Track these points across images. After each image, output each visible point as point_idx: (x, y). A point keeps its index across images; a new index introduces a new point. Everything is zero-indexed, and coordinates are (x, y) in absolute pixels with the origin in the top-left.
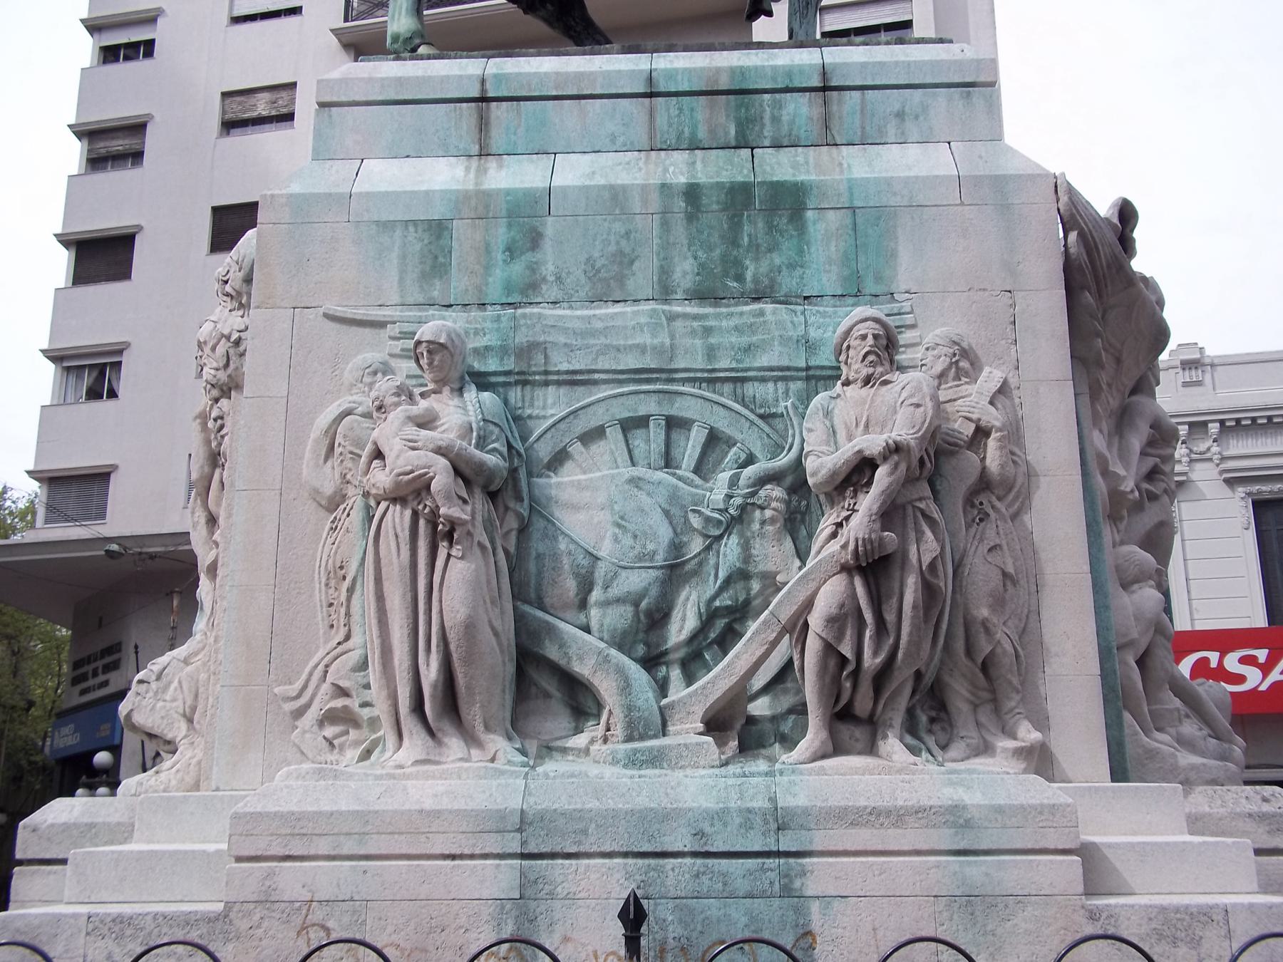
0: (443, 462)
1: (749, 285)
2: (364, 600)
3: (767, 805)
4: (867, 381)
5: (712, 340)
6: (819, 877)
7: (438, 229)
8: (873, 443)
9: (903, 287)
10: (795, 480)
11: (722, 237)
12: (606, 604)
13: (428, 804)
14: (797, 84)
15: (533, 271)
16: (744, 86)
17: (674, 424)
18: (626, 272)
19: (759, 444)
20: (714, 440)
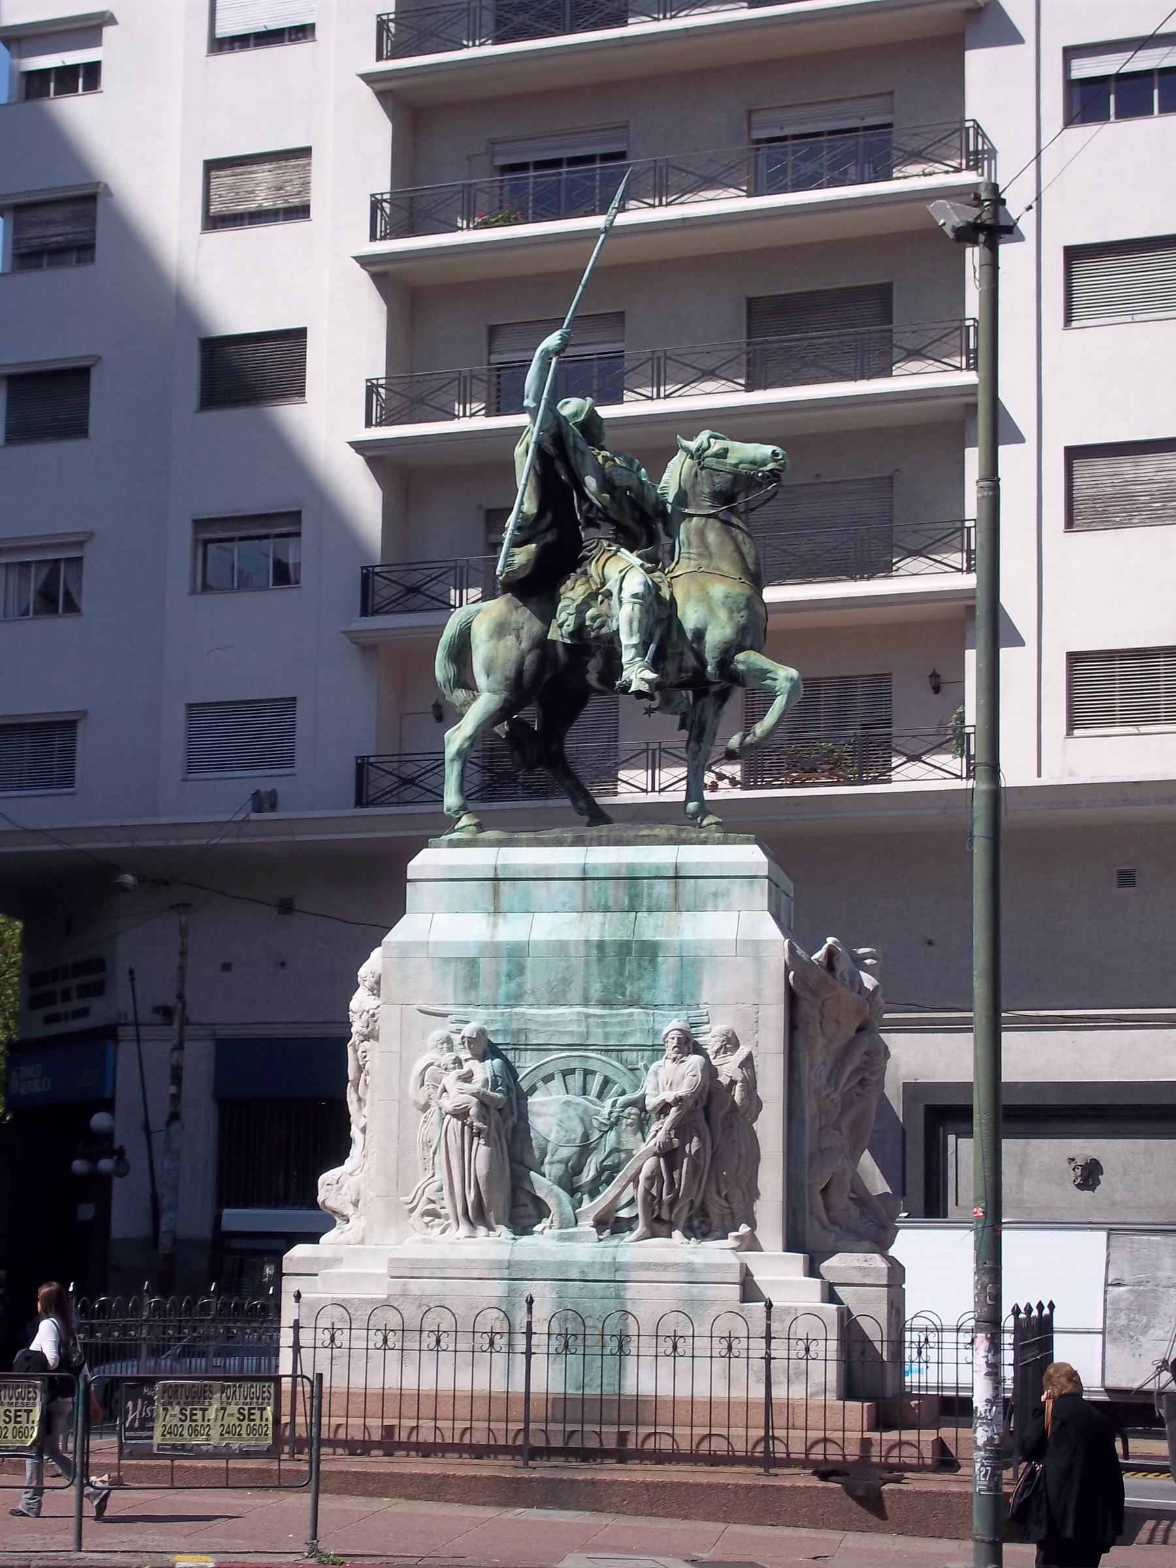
0: (475, 1100)
1: (628, 998)
2: (441, 1157)
4: (674, 1060)
6: (632, 1291)
7: (473, 963)
8: (669, 1096)
10: (640, 1103)
12: (551, 1163)
13: (470, 1257)
17: (587, 1073)
20: (606, 1082)
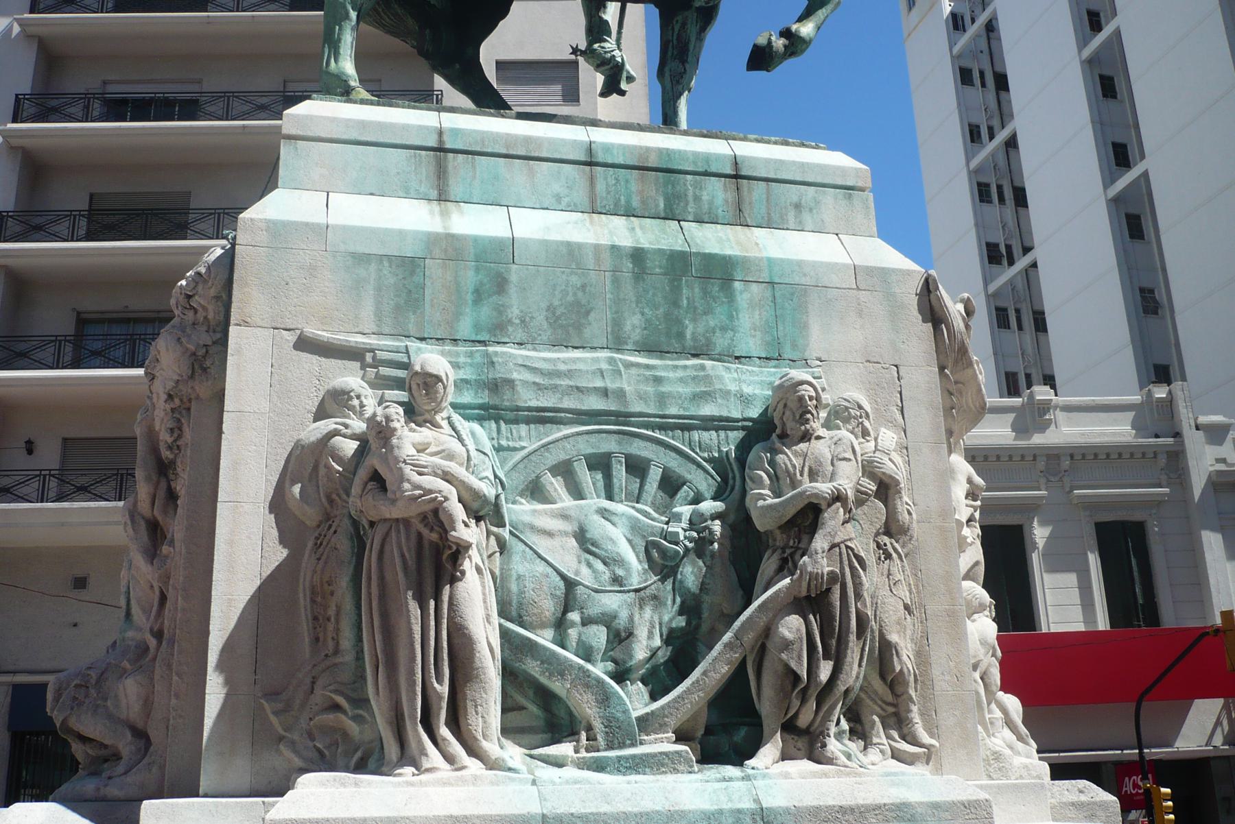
3: (754, 806)
5: (663, 389)
7: (409, 266)
9: (815, 355)
11: (665, 298)
14: (713, 169)
15: (500, 313)
16: (670, 166)
18: (583, 321)
19: (705, 484)
